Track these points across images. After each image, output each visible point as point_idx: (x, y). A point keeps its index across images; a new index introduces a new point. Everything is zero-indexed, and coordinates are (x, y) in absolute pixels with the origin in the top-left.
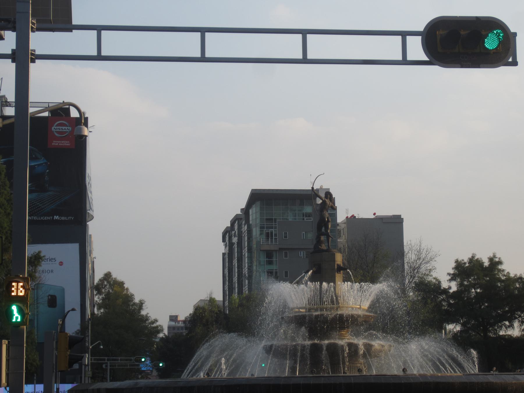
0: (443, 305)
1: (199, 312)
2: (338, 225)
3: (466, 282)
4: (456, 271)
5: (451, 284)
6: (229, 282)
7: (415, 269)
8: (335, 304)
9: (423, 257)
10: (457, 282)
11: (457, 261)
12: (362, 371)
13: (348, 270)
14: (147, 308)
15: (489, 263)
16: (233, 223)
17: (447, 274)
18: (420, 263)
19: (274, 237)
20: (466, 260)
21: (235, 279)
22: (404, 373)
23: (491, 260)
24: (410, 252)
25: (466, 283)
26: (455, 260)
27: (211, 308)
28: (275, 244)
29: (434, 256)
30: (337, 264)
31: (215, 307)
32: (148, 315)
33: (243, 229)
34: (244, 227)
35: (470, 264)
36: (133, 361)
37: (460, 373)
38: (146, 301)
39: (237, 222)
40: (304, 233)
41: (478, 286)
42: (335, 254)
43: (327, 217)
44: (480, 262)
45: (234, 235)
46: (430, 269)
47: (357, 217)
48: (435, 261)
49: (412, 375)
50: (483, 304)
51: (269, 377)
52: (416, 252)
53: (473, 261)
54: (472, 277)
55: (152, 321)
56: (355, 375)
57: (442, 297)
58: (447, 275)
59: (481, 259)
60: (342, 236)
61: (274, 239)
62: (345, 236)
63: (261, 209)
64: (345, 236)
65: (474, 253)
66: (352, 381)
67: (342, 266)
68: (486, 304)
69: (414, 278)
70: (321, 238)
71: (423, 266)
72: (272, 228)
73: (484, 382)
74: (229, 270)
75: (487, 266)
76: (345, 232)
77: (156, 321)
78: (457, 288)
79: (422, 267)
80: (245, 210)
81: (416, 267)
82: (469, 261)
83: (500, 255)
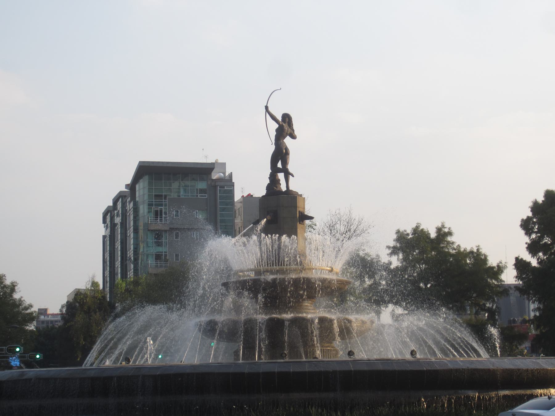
5: (392, 258)
6: (110, 267)
8: (299, 265)
11: (398, 232)
14: (20, 291)
15: (436, 235)
16: (115, 201)
20: (409, 231)
21: (118, 264)
23: (439, 230)
27: (93, 294)
28: (164, 224)
30: (299, 211)
32: (22, 299)
39: (121, 199)
42: (297, 196)
43: (285, 147)
48: (368, 232)
55: (25, 307)
60: (238, 217)
62: (241, 217)
63: (150, 184)
64: (241, 217)
72: (161, 205)
74: (110, 254)
76: (241, 212)
80: (130, 186)
83: (449, 225)
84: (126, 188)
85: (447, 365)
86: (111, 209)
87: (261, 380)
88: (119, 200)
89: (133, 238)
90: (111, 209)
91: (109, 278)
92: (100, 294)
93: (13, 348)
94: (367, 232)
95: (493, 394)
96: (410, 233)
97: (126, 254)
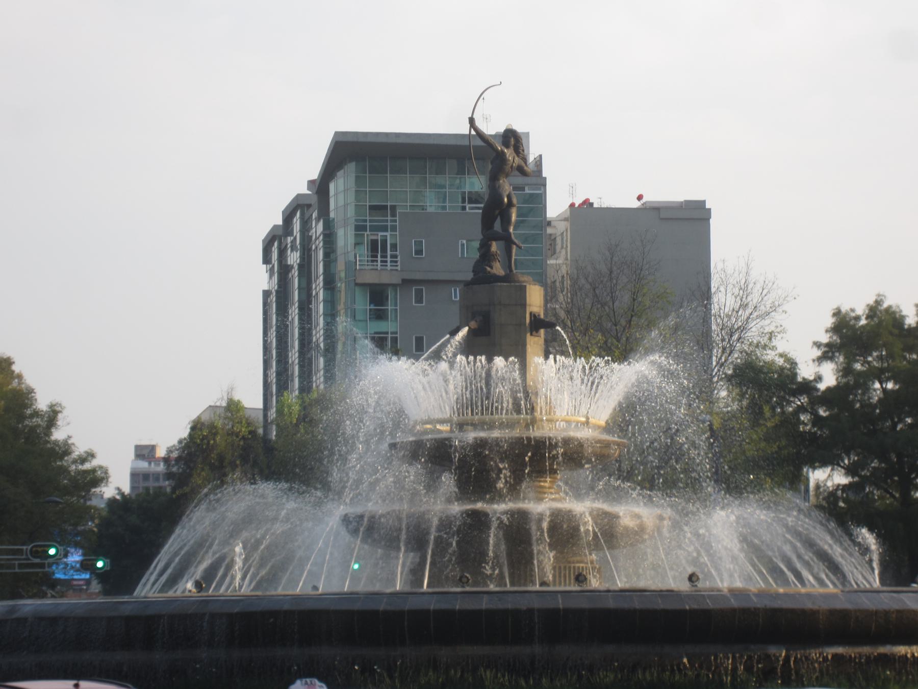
0: (799, 422)
1: (200, 436)
2: (549, 223)
3: (859, 364)
4: (835, 338)
7: (734, 332)
9: (755, 301)
10: (836, 363)
11: (837, 313)
12: (586, 579)
13: (558, 328)
14: (69, 424)
16: (288, 217)
17: (811, 344)
18: (746, 317)
19: (389, 253)
20: (861, 310)
21: (294, 356)
22: (693, 586)
24: (722, 289)
25: (858, 366)
26: (834, 309)
27: (230, 426)
28: (391, 270)
29: (781, 300)
30: (531, 313)
31: (241, 423)
32: (70, 442)
33: (314, 230)
34: (316, 226)
35: (869, 320)
36: (27, 555)
37: (821, 583)
38: (64, 407)
40: (465, 242)
41: (889, 374)
42: (525, 286)
43: (507, 193)
44: (895, 315)
45: (292, 247)
46: (770, 331)
47: (595, 206)
49: (713, 591)
50: (901, 420)
51: (352, 593)
52: (737, 289)
53: (878, 313)
54: (876, 352)
56: (568, 588)
57: (800, 400)
58: (812, 347)
59: (898, 307)
60: (560, 252)
61: (389, 256)
62: (566, 253)
64: (566, 253)
65: (881, 293)
66: (560, 604)
67: (542, 316)
68: (909, 420)
69: (732, 355)
70: (490, 246)
71: (753, 324)
72: (385, 229)
73: (892, 610)
75: (912, 326)
76: (567, 241)
77: (91, 455)
78: (837, 379)
79: (751, 328)
81: (736, 327)
82: (867, 312)
84: (308, 189)
85: (730, 600)
86: (280, 232)
87: (406, 623)
88: (295, 214)
89: (325, 301)
90: (280, 232)
91: (276, 386)
92: (246, 427)
93: (42, 549)
94: (780, 310)
95: (814, 654)
96: (863, 315)
97: (310, 335)
